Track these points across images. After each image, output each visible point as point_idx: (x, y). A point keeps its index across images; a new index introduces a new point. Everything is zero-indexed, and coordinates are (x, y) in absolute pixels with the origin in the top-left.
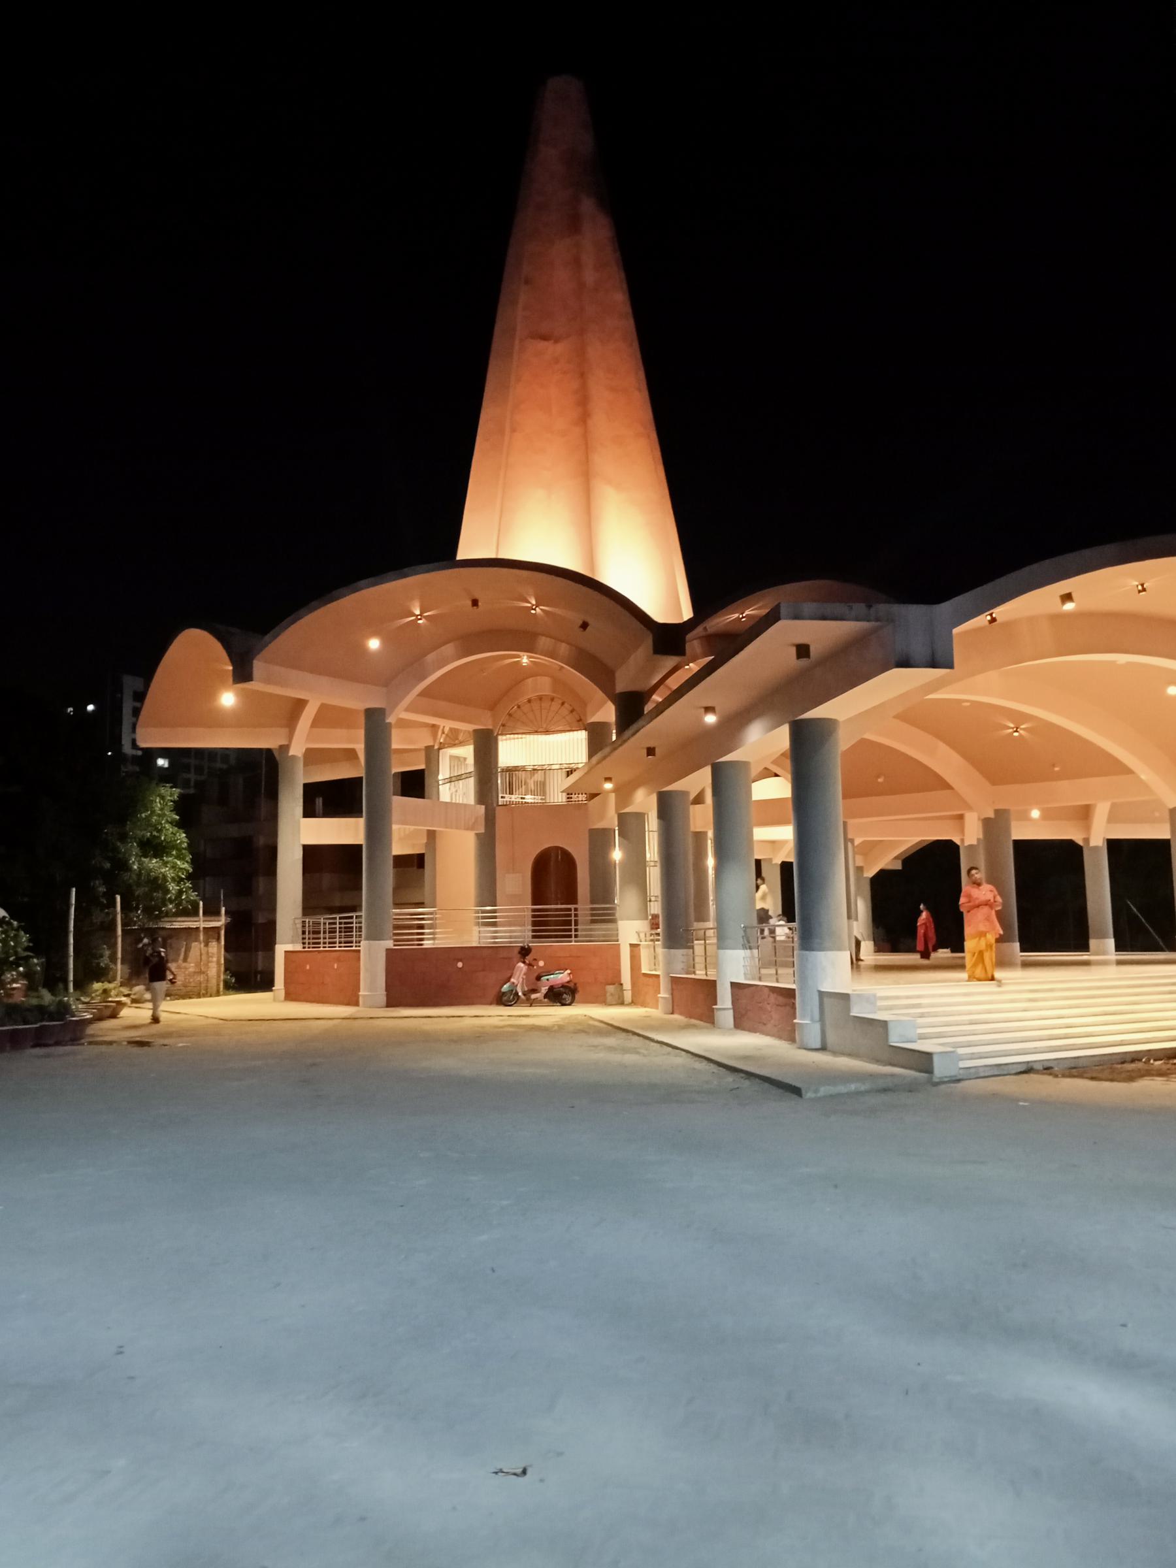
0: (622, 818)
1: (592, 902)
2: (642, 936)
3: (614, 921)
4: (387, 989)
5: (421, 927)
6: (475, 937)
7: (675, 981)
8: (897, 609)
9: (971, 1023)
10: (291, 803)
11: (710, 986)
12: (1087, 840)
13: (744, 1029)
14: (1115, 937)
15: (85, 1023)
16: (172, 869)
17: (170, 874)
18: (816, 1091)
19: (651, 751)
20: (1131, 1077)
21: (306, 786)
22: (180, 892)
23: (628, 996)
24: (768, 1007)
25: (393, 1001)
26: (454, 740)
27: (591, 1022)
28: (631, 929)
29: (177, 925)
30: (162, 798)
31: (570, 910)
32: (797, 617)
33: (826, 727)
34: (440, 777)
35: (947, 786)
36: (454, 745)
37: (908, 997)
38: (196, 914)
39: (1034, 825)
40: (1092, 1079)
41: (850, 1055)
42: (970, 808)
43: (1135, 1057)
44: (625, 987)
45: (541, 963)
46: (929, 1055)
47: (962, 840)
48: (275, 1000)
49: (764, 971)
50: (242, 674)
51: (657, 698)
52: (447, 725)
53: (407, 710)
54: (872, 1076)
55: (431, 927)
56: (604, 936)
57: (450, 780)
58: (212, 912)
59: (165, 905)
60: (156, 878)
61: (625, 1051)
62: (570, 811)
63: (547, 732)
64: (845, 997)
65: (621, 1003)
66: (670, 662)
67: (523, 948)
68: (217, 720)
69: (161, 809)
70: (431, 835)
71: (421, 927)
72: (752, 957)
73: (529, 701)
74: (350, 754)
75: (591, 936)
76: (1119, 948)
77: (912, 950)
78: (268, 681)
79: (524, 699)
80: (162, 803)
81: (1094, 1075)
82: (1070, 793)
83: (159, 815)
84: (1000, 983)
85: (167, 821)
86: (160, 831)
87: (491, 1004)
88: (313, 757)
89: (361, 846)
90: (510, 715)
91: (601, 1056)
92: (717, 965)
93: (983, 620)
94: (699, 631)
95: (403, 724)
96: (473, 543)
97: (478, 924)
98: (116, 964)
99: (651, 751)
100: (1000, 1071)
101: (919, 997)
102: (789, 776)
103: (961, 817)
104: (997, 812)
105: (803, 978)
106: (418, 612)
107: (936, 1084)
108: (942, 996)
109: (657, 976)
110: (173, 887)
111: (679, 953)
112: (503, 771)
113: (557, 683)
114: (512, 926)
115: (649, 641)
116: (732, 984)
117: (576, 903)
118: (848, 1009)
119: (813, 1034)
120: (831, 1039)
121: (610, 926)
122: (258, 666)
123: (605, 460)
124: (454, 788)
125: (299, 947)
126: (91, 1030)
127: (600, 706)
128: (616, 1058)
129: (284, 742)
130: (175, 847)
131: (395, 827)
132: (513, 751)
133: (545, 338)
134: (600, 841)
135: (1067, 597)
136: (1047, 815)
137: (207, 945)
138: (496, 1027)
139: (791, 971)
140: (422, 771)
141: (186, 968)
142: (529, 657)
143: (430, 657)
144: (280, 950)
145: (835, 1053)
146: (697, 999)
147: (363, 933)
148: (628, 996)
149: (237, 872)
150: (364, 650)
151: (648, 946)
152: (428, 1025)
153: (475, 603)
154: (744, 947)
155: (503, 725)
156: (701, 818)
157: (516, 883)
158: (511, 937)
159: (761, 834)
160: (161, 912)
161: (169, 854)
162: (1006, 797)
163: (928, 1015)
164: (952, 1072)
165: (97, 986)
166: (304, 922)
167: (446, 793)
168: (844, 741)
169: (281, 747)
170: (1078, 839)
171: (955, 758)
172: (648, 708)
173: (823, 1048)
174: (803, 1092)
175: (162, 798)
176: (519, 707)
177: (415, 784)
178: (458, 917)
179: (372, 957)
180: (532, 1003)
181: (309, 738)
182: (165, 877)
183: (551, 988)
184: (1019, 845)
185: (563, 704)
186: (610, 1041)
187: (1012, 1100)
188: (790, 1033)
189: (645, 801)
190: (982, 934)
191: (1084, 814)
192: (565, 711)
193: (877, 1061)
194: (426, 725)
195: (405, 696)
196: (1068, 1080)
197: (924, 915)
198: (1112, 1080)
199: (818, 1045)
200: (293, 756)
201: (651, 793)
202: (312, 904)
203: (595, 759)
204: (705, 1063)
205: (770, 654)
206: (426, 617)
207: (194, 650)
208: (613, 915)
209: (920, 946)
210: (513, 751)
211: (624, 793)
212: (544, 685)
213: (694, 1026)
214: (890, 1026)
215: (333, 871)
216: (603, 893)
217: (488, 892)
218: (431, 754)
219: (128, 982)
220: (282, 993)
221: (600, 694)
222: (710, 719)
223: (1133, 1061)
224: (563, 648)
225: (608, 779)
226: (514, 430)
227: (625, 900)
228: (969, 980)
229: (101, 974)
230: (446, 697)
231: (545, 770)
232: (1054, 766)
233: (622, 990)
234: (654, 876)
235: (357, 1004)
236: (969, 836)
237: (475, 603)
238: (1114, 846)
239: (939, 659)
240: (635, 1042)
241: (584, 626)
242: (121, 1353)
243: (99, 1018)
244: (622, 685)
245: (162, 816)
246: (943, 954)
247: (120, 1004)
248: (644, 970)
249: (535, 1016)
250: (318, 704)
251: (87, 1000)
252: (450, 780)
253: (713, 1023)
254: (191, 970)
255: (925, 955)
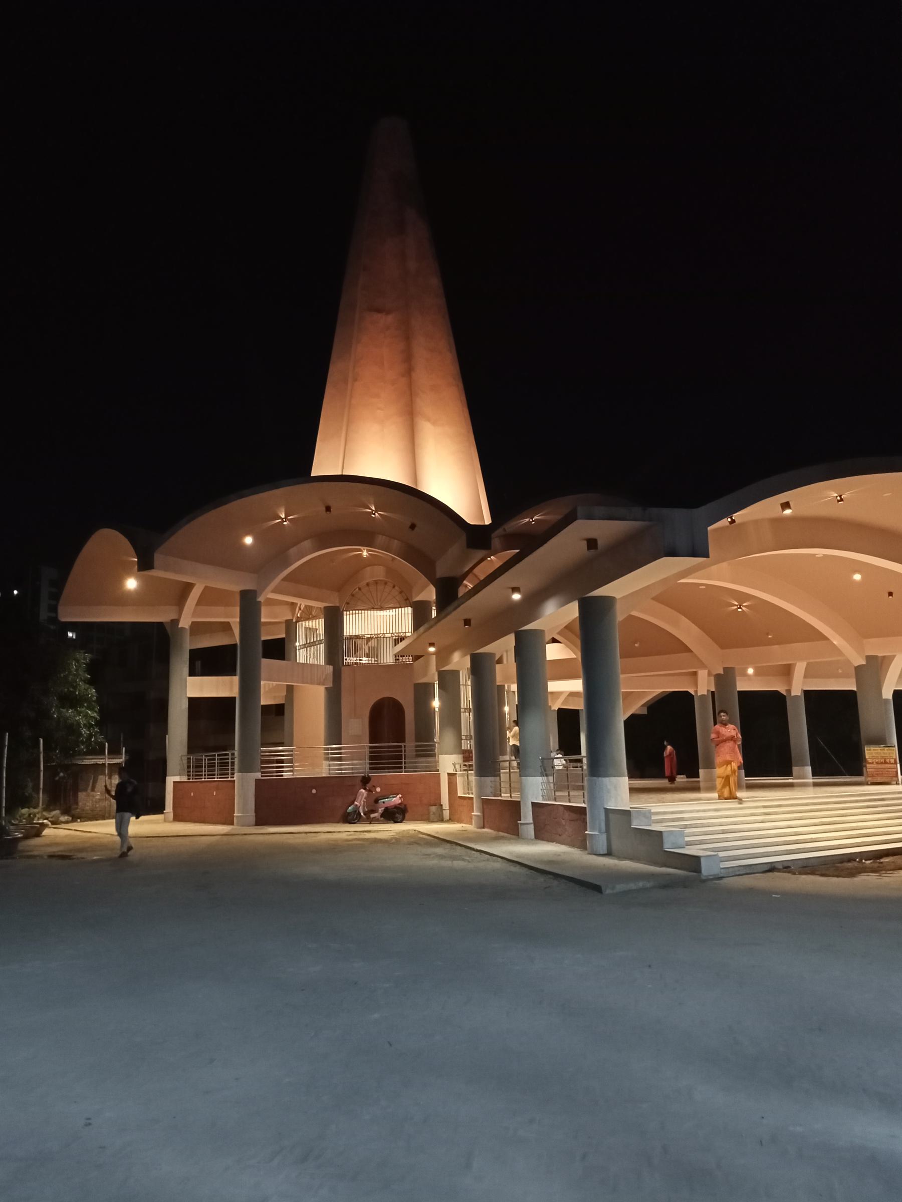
0: (442, 675)
1: (417, 741)
2: (458, 767)
3: (434, 755)
4: (256, 812)
5: (282, 761)
6: (324, 769)
7: (485, 803)
8: (665, 511)
9: (724, 832)
10: (180, 666)
11: (514, 807)
12: (789, 691)
13: (543, 840)
14: (811, 765)
15: (18, 840)
16: (85, 717)
17: (83, 722)
18: (613, 888)
19: (467, 622)
20: (852, 874)
21: (191, 651)
22: (90, 736)
23: (446, 814)
24: (563, 822)
25: (261, 820)
26: (308, 615)
27: (421, 836)
28: (448, 763)
29: (86, 762)
30: (77, 661)
31: (401, 747)
32: (590, 517)
33: (608, 602)
34: (297, 644)
35: (687, 650)
36: (308, 619)
37: (673, 813)
38: (102, 752)
39: (750, 680)
40: (822, 875)
41: (631, 859)
42: (703, 666)
43: (850, 858)
44: (444, 807)
45: (378, 790)
46: (697, 859)
47: (696, 692)
48: (165, 821)
49: (558, 794)
50: (145, 564)
51: (469, 584)
52: (302, 603)
53: (274, 591)
54: (652, 876)
55: (291, 761)
56: (426, 767)
57: (305, 646)
58: (114, 752)
59: (78, 746)
60: (72, 724)
61: (454, 858)
62: (398, 669)
63: (381, 608)
64: (627, 814)
65: (441, 820)
66: (480, 554)
67: (364, 778)
68: (125, 600)
69: (76, 670)
70: (290, 689)
71: (282, 761)
72: (548, 782)
73: (368, 584)
74: (226, 627)
75: (416, 767)
76: (815, 774)
77: (662, 776)
78: (166, 568)
79: (364, 583)
80: (78, 665)
81: (823, 872)
82: (778, 654)
83: (75, 675)
84: (740, 801)
85: (81, 680)
86: (75, 688)
87: (338, 822)
88: (197, 628)
89: (235, 698)
90: (353, 595)
91: (434, 862)
92: (521, 790)
93: (725, 522)
94: (499, 531)
95: (270, 602)
96: (324, 464)
97: (327, 759)
98: (38, 793)
99: (467, 622)
100: (750, 870)
101: (681, 812)
102: (579, 642)
103: (695, 674)
104: (724, 669)
105: (593, 798)
106: (283, 516)
107: (704, 881)
108: (698, 811)
109: (472, 798)
110: (85, 731)
111: (489, 780)
112: (347, 638)
113: (390, 571)
114: (352, 759)
115: (463, 539)
116: (533, 803)
117: (404, 741)
118: (630, 823)
119: (601, 844)
120: (616, 845)
121: (430, 759)
122: (158, 558)
123: (425, 404)
124: (309, 653)
125: (185, 779)
126: (22, 845)
127: (424, 587)
128: (447, 863)
129: (173, 616)
130: (88, 700)
131: (262, 683)
132: (354, 623)
133: (379, 311)
134: (423, 692)
135: (786, 505)
136: (759, 672)
137: (110, 778)
138: (347, 840)
139: (581, 793)
140: (283, 639)
141: (93, 796)
142: (368, 551)
143: (293, 551)
144: (170, 780)
145: (620, 858)
146: (505, 817)
147: (236, 767)
148: (446, 814)
149: (136, 718)
150: (243, 546)
151: (462, 775)
152: (291, 839)
153: (328, 509)
154: (542, 775)
155: (348, 603)
156: (506, 675)
157: (356, 726)
158: (352, 769)
159: (553, 686)
160: (74, 751)
161: (82, 706)
162: (732, 658)
163: (691, 826)
164: (715, 871)
165: (25, 811)
166: (189, 759)
167: (302, 656)
168: (620, 614)
169: (172, 620)
170: (782, 689)
171: (694, 629)
172: (462, 591)
173: (609, 854)
174: (603, 889)
175: (77, 661)
176: (360, 589)
177: (278, 649)
178: (312, 753)
179: (244, 786)
180: (371, 821)
181: (194, 614)
182: (79, 724)
183: (386, 809)
184: (743, 695)
185: (394, 587)
186: (439, 850)
187: (765, 893)
188: (582, 843)
189: (460, 662)
190: (729, 763)
191: (787, 671)
192: (395, 592)
193: (655, 864)
194: (287, 603)
195: (274, 578)
196: (804, 876)
197: (669, 748)
198: (838, 876)
199: (606, 852)
200: (182, 628)
201: (465, 655)
202: (195, 744)
203: (422, 629)
204: (518, 866)
205: (567, 546)
206: (289, 520)
207: (108, 543)
208: (434, 750)
209: (667, 772)
210: (354, 623)
211: (443, 655)
212: (379, 572)
213: (502, 838)
214: (665, 835)
215: (210, 717)
216: (425, 733)
217: (335, 733)
218: (290, 627)
219: (48, 808)
220: (171, 815)
221: (424, 579)
222: (516, 597)
223: (849, 861)
224: (396, 543)
225: (432, 645)
226: (355, 380)
227: (442, 737)
228: (719, 799)
229: (27, 802)
230: (302, 582)
231: (378, 638)
232: (768, 634)
233: (442, 810)
234: (467, 719)
235: (232, 823)
236: (703, 686)
237: (328, 509)
238: (807, 694)
239: (699, 550)
240: (459, 851)
241: (413, 527)
242: (90, 1124)
243: (27, 837)
244: (442, 571)
245: (77, 675)
246: (681, 779)
247: (44, 826)
248: (460, 793)
249: (375, 831)
250: (202, 588)
251: (17, 822)
252: (305, 646)
253: (518, 835)
254: (98, 797)
255: (672, 779)
